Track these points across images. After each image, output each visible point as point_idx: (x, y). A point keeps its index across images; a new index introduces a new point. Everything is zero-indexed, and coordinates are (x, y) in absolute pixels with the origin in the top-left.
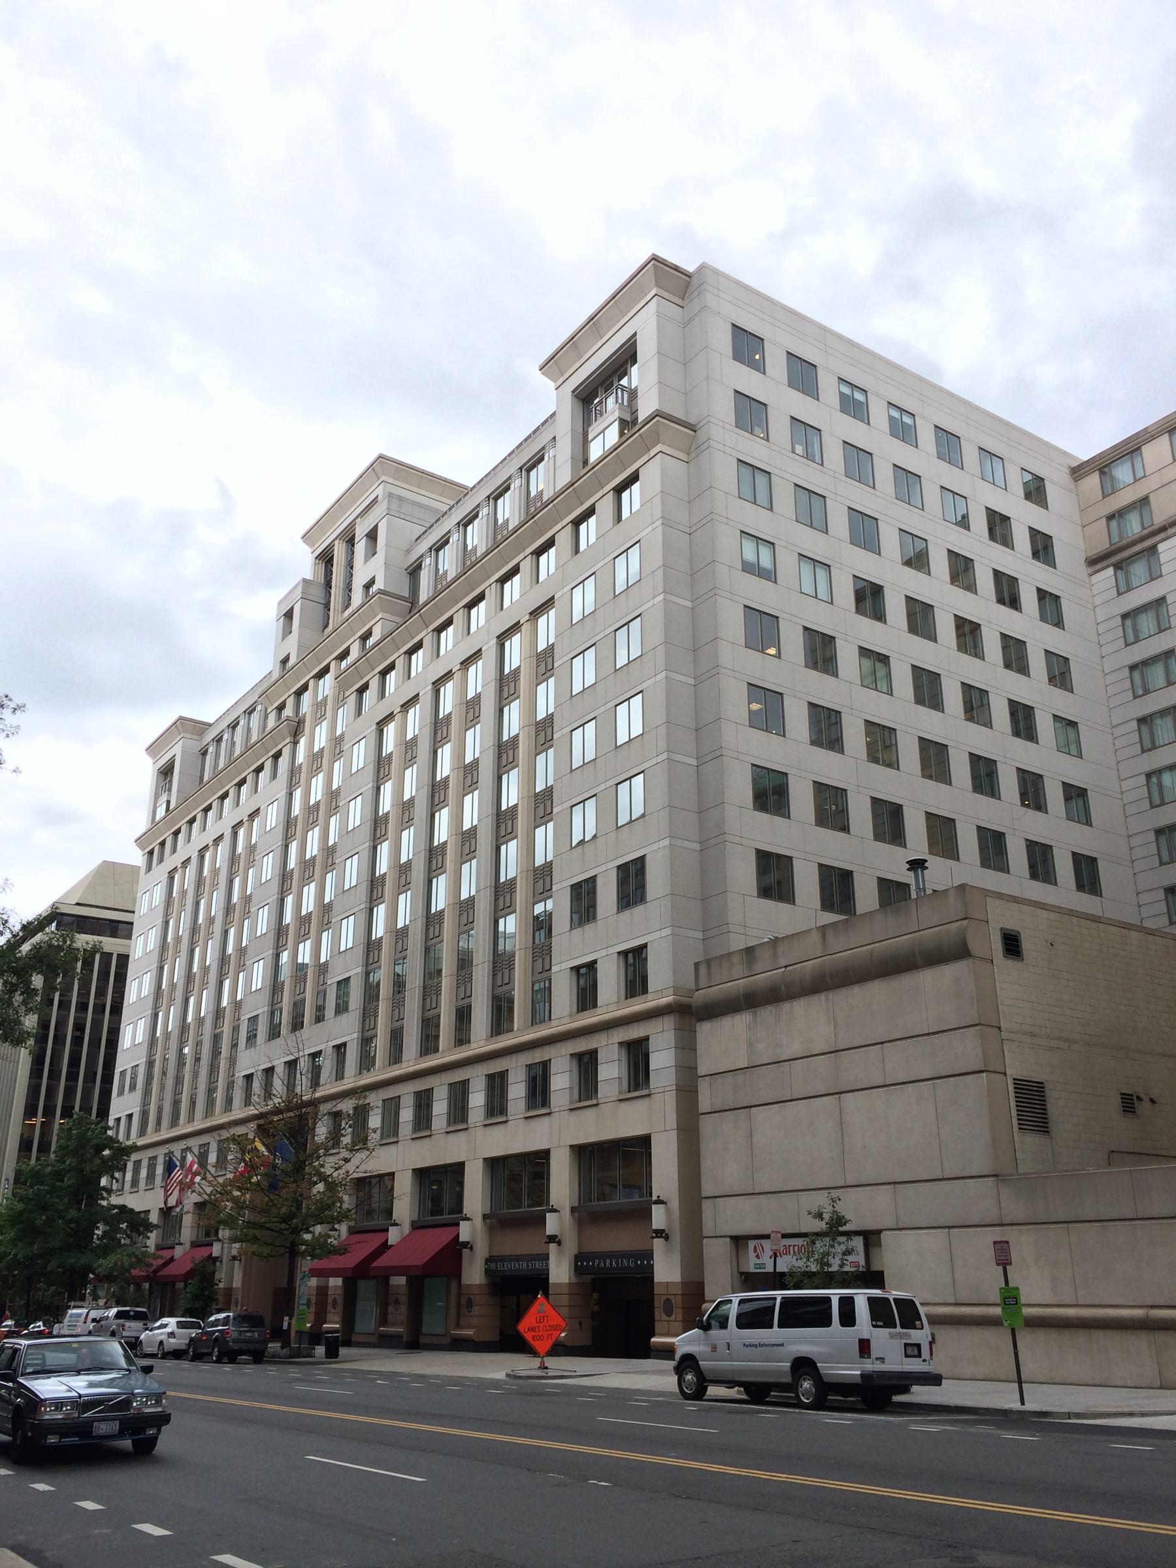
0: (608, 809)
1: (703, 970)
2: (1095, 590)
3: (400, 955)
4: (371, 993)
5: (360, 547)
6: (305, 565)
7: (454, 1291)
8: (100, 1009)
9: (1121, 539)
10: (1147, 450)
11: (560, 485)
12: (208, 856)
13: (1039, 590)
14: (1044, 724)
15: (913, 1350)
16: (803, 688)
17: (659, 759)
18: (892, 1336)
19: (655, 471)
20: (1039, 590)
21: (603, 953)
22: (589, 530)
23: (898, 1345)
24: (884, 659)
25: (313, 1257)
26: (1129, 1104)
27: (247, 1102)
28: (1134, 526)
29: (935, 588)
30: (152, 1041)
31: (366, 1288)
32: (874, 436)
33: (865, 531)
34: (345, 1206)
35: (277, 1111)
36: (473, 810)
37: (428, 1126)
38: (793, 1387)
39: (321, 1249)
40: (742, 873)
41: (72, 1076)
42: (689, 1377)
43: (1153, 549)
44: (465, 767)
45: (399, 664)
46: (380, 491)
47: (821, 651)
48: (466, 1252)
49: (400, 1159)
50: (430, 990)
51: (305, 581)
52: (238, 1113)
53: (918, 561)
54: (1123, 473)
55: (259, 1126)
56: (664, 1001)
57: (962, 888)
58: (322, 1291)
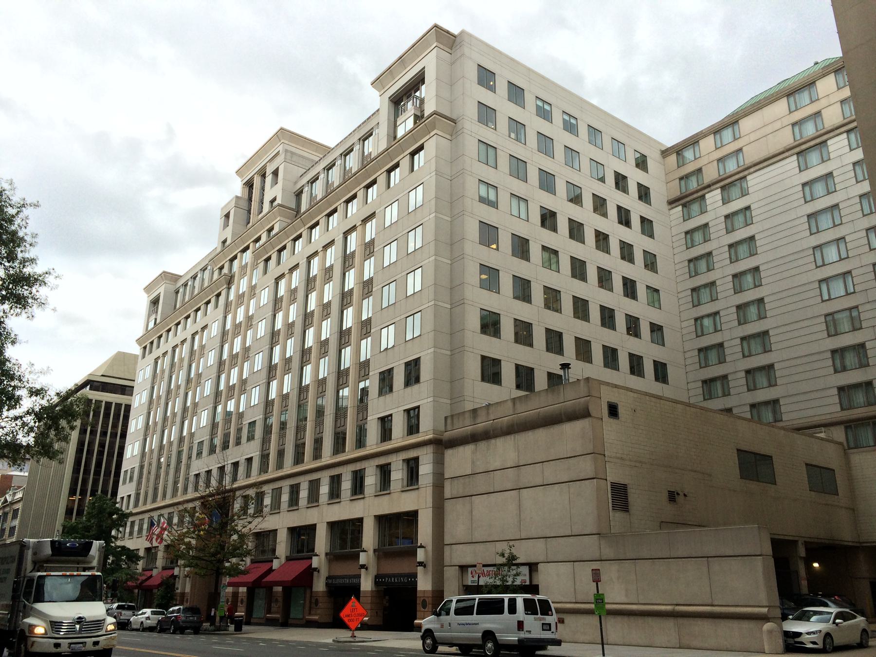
0: (401, 332)
1: (449, 421)
2: (672, 218)
3: (284, 409)
4: (267, 430)
5: (269, 179)
6: (237, 188)
7: (308, 596)
8: (113, 435)
9: (801, 138)
10: (702, 143)
11: (381, 149)
12: (177, 350)
13: (641, 217)
14: (641, 291)
15: (547, 627)
16: (510, 266)
17: (430, 304)
18: (535, 619)
19: (432, 144)
20: (641, 217)
21: (396, 410)
22: (396, 176)
23: (539, 623)
24: (556, 253)
25: (230, 576)
26: (672, 497)
27: (196, 489)
28: (693, 184)
29: (585, 214)
30: (143, 454)
31: (261, 592)
32: (555, 130)
33: (547, 182)
34: (250, 548)
35: (211, 495)
36: (327, 329)
37: (297, 504)
38: (482, 647)
39: (235, 571)
40: (473, 368)
41: (97, 473)
42: (428, 641)
43: (703, 197)
44: (324, 305)
45: (289, 246)
46: (281, 148)
47: (521, 247)
48: (315, 573)
49: (281, 522)
50: (300, 429)
51: (237, 197)
52: (190, 495)
53: (576, 199)
54: (689, 154)
55: (202, 503)
56: (430, 436)
57: (588, 379)
58: (235, 595)
